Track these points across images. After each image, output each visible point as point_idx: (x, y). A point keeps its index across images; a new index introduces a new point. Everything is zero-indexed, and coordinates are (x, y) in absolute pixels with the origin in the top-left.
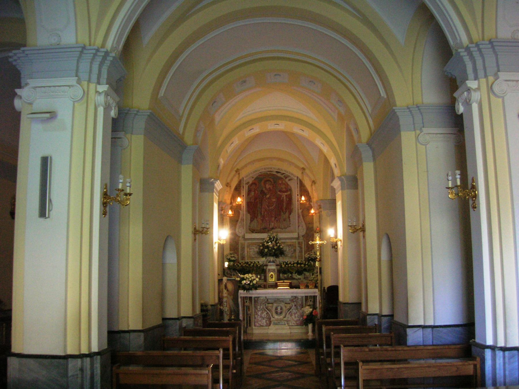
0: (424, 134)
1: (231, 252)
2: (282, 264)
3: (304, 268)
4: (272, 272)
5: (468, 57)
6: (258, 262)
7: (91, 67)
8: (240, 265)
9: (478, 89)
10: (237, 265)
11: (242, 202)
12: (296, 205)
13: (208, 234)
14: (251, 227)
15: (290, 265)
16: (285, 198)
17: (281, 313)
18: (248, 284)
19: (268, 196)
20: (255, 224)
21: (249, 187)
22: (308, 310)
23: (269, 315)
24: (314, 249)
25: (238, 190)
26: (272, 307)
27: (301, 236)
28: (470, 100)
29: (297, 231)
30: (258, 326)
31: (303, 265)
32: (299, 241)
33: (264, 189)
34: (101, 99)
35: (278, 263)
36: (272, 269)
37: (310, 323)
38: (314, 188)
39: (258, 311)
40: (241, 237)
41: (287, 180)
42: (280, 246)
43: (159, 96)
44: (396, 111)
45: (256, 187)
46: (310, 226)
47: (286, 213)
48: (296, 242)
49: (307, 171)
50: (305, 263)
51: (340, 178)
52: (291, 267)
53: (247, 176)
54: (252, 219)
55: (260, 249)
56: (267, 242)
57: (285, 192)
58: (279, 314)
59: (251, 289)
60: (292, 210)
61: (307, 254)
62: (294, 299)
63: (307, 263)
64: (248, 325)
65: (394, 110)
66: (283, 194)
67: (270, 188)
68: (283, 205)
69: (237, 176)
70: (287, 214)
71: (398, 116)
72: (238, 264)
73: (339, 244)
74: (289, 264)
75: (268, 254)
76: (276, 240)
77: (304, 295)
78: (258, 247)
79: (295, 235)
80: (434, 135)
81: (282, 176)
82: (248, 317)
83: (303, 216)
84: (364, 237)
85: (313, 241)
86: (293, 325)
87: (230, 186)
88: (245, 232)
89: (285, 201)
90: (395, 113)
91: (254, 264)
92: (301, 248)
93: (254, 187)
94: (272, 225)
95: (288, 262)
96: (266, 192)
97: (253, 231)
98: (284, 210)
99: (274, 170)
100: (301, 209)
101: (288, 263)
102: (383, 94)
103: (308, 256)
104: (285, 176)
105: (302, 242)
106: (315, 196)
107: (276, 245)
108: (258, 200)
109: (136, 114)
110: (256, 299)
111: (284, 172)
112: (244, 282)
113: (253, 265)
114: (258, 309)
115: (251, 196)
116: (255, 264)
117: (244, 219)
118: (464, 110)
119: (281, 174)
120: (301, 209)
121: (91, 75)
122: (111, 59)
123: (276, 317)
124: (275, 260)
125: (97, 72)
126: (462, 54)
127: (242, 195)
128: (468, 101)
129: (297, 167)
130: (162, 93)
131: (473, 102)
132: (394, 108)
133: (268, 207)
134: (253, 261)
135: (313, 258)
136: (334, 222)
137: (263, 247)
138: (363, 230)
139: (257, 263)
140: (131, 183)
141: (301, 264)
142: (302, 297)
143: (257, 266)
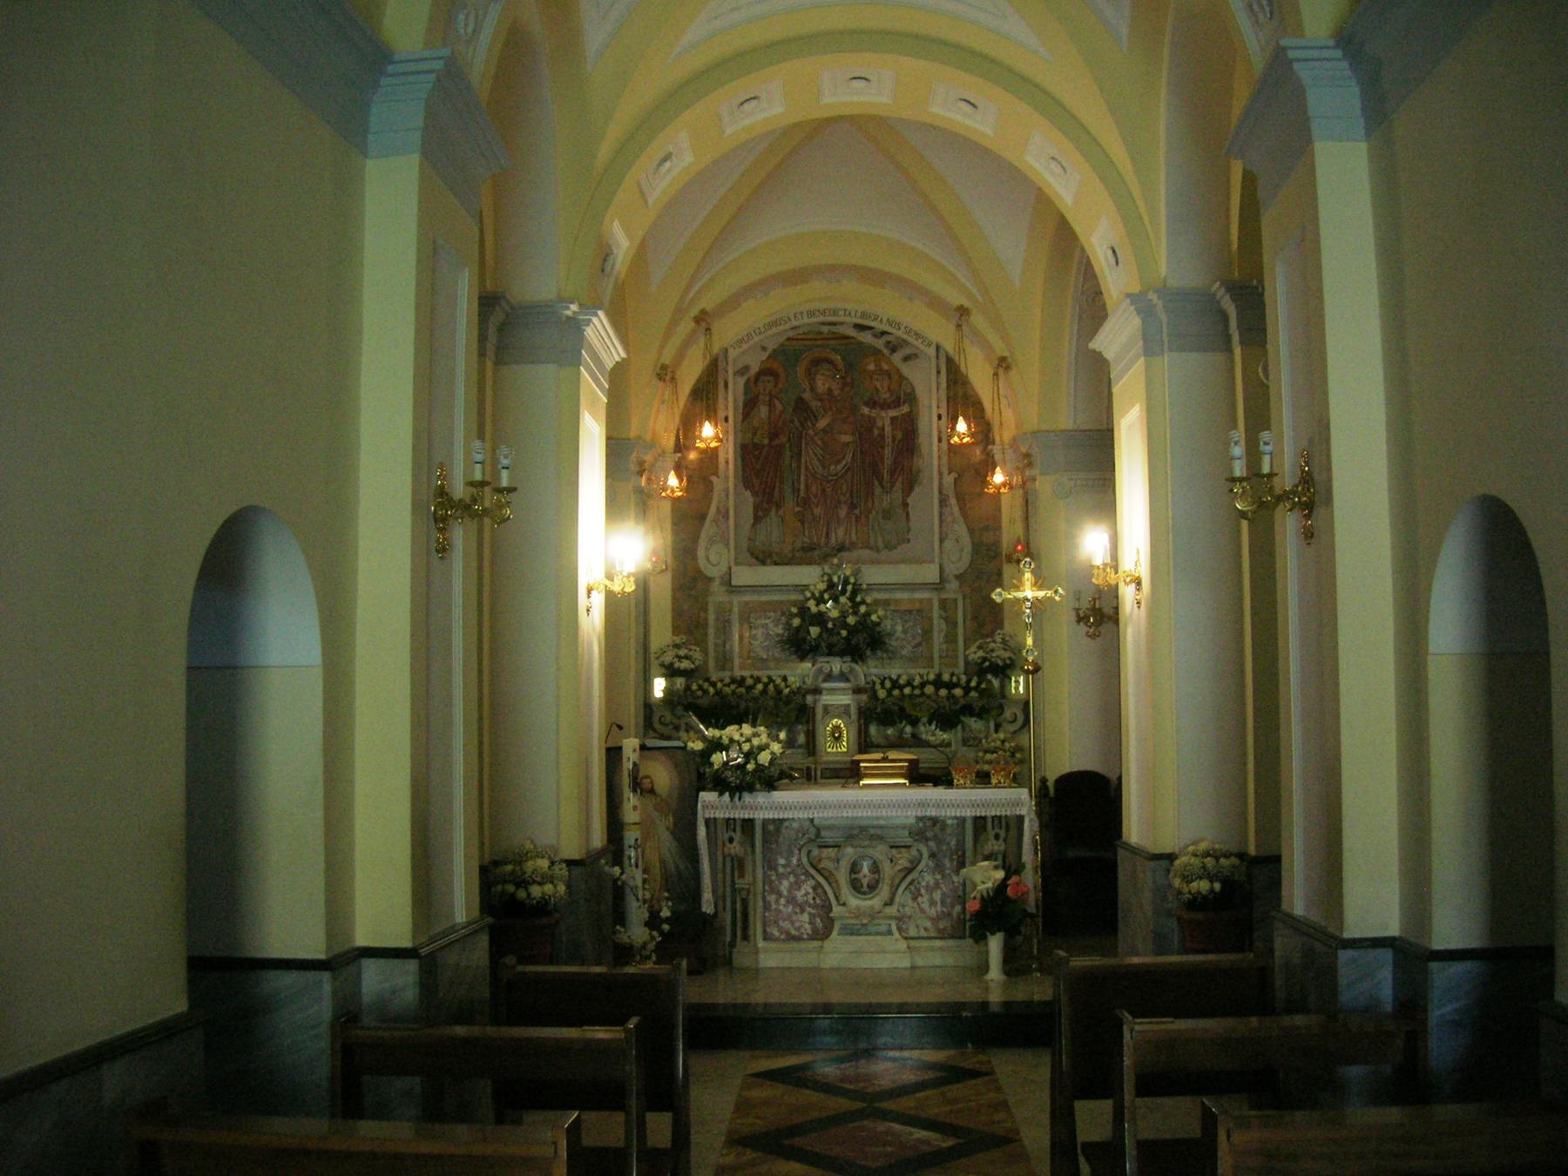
1: (678, 640)
2: (878, 687)
3: (962, 701)
6: (785, 679)
8: (711, 690)
10: (700, 687)
11: (720, 440)
15: (907, 691)
16: (888, 429)
17: (873, 887)
19: (822, 424)
20: (772, 532)
24: (1002, 629)
25: (704, 398)
27: (951, 578)
31: (958, 692)
32: (944, 596)
33: (807, 395)
35: (862, 682)
39: (781, 877)
41: (897, 358)
42: (868, 614)
45: (775, 387)
47: (895, 489)
48: (930, 601)
49: (978, 320)
50: (969, 681)
52: (911, 696)
54: (760, 513)
55: (788, 624)
56: (820, 601)
57: (889, 407)
61: (973, 648)
63: (973, 684)
64: (739, 933)
69: (702, 340)
70: (897, 494)
76: (855, 592)
77: (969, 813)
79: (930, 573)
81: (879, 344)
88: (732, 563)
89: (889, 440)
91: (766, 685)
92: (952, 623)
94: (839, 534)
95: (899, 676)
96: (814, 409)
97: (763, 557)
99: (847, 319)
101: (902, 682)
103: (981, 653)
106: (1007, 424)
107: (855, 613)
108: (783, 439)
112: (719, 758)
113: (765, 691)
114: (781, 870)
116: (771, 687)
117: (727, 511)
119: (875, 336)
123: (854, 902)
124: (852, 670)
127: (721, 414)
129: (936, 303)
134: (763, 675)
135: (1000, 663)
139: (778, 681)
141: (950, 686)
142: (962, 821)
143: (779, 691)
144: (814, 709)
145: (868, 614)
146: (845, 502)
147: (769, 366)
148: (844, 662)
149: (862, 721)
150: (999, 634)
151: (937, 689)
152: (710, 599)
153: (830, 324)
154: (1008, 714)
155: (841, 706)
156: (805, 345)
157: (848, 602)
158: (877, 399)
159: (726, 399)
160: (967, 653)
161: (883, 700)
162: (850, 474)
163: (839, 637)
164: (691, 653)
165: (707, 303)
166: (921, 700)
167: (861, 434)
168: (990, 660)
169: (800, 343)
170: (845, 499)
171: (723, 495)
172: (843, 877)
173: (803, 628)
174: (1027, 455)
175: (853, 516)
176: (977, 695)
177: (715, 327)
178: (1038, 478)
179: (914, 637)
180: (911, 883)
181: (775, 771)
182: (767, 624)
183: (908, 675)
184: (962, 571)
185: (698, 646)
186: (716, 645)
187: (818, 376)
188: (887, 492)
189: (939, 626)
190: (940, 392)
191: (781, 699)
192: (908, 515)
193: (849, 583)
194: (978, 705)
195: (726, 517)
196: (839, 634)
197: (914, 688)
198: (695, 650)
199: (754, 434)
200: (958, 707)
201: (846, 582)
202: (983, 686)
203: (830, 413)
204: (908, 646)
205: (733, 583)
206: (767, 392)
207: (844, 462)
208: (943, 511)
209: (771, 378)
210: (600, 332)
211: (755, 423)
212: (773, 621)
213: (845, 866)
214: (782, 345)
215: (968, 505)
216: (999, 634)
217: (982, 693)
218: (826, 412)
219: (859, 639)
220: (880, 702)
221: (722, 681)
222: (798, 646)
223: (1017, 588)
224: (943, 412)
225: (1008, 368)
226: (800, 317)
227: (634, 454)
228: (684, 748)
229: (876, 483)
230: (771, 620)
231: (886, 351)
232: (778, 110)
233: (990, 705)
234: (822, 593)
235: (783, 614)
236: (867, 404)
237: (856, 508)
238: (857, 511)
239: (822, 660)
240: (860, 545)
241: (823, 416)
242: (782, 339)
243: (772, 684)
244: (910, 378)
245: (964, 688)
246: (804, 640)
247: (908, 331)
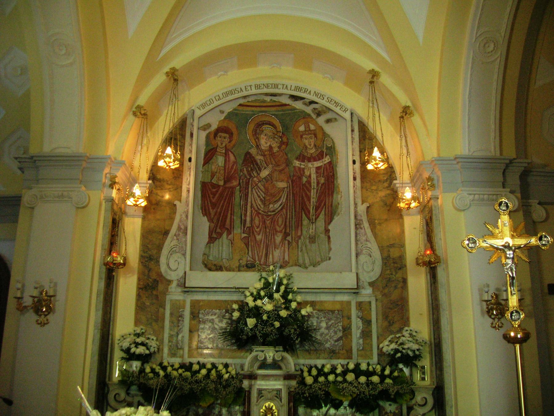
2: (306, 374)
3: (380, 388)
4: (271, 400)
8: (162, 373)
10: (153, 370)
14: (211, 258)
15: (331, 378)
16: (314, 176)
19: (265, 173)
21: (208, 137)
24: (409, 326)
27: (366, 284)
29: (354, 270)
32: (360, 299)
33: (253, 151)
35: (292, 369)
40: (174, 284)
41: (321, 121)
42: (297, 311)
45: (230, 142)
47: (318, 219)
48: (349, 303)
49: (385, 79)
50: (383, 370)
52: (335, 382)
54: (214, 235)
60: (337, 207)
61: (386, 343)
63: (387, 372)
66: (310, 165)
70: (321, 223)
74: (329, 373)
79: (349, 280)
81: (308, 110)
83: (372, 224)
88: (188, 269)
91: (209, 371)
92: (367, 322)
93: (222, 141)
95: (323, 366)
101: (326, 370)
103: (393, 346)
104: (314, 109)
107: (287, 308)
108: (235, 183)
111: (315, 99)
113: (208, 376)
115: (214, 168)
116: (213, 372)
117: (186, 229)
119: (305, 104)
124: (283, 358)
133: (263, 202)
135: (411, 354)
137: (242, 314)
139: (220, 367)
141: (369, 374)
143: (220, 376)
144: (249, 392)
146: (281, 232)
147: (225, 124)
148: (277, 351)
149: (292, 404)
150: (407, 330)
151: (357, 377)
152: (168, 297)
154: (419, 398)
155: (273, 390)
156: (253, 111)
157: (281, 299)
158: (306, 154)
159: (191, 145)
160: (381, 346)
161: (311, 385)
162: (284, 211)
163: (272, 328)
164: (147, 341)
165: (178, 62)
166: (345, 385)
167: (293, 181)
168: (401, 352)
169: (250, 108)
170: (281, 229)
171: (184, 216)
173: (242, 320)
174: (430, 179)
175: (286, 242)
176: (391, 381)
178: (440, 197)
179: (335, 333)
182: (213, 319)
183: (332, 365)
184: (374, 279)
185: (155, 336)
186: (171, 336)
187: (262, 136)
188: (313, 223)
190: (354, 144)
191: (220, 383)
192: (329, 238)
193: (283, 284)
194: (393, 391)
196: (273, 325)
198: (153, 339)
199: (213, 176)
200: (376, 393)
201: (280, 284)
202: (396, 374)
203: (270, 166)
204: (331, 340)
205: (187, 285)
206: (224, 145)
207: (280, 203)
208: (358, 232)
209: (227, 136)
211: (214, 168)
212: (218, 317)
214: (235, 109)
215: (378, 227)
216: (407, 330)
218: (268, 166)
219: (291, 331)
220: (308, 387)
221: (172, 366)
226: (250, 89)
227: (107, 170)
229: (304, 215)
230: (217, 316)
231: (314, 116)
236: (297, 159)
237: (289, 235)
238: (289, 238)
239: (257, 349)
240: (291, 264)
241: (265, 168)
242: (234, 105)
243: (214, 370)
244: (332, 136)
245: (379, 376)
246: (242, 331)
247: (330, 100)
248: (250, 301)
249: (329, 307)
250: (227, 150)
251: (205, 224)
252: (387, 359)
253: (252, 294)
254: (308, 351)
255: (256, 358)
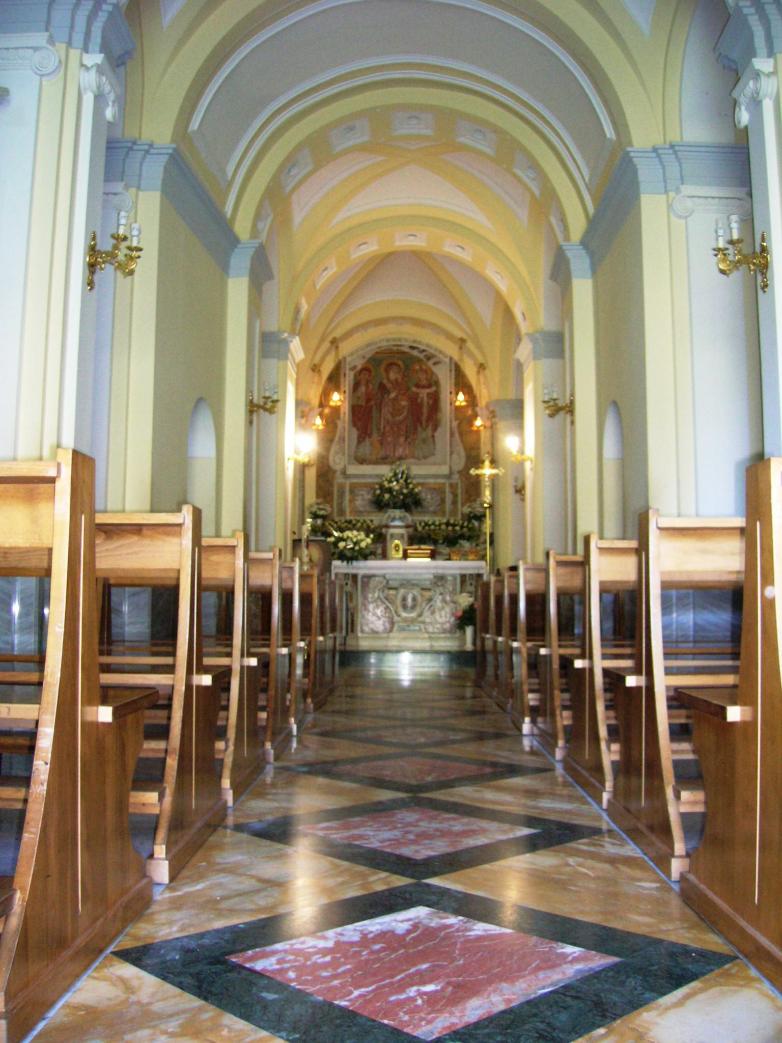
0: (684, 197)
1: (319, 501)
2: (418, 525)
3: (459, 533)
5: (756, 17)
6: (372, 521)
7: (73, 20)
9: (775, 73)
11: (342, 401)
12: (446, 412)
13: (274, 413)
15: (432, 527)
17: (413, 607)
18: (351, 549)
19: (393, 395)
20: (366, 449)
21: (355, 375)
22: (465, 600)
23: (390, 610)
25: (334, 380)
26: (396, 596)
28: (758, 94)
29: (448, 463)
30: (367, 633)
31: (458, 528)
33: (385, 381)
34: (90, 79)
36: (398, 534)
37: (468, 625)
38: (482, 380)
39: (369, 603)
41: (430, 363)
42: (413, 489)
43: (190, 130)
44: (632, 154)
45: (370, 376)
46: (474, 453)
48: (444, 484)
49: (470, 345)
51: (532, 337)
52: (434, 530)
53: (352, 354)
54: (361, 439)
55: (374, 494)
56: (390, 481)
58: (409, 609)
59: (356, 559)
61: (466, 507)
62: (440, 579)
64: (350, 630)
65: (628, 153)
67: (396, 380)
68: (422, 413)
69: (333, 353)
70: (429, 431)
71: (634, 166)
72: (332, 523)
73: (528, 465)
75: (391, 503)
76: (407, 478)
77: (457, 572)
78: (372, 491)
79: (445, 470)
80: (702, 200)
81: (421, 356)
82: (349, 614)
83: (461, 434)
84: (572, 423)
85: (477, 468)
86: (436, 630)
87: (319, 371)
88: (346, 463)
89: (425, 404)
90: (630, 160)
91: (362, 524)
92: (455, 495)
94: (400, 451)
97: (362, 461)
98: (424, 422)
100: (456, 419)
102: (610, 133)
103: (469, 510)
105: (457, 484)
106: (484, 396)
107: (407, 488)
108: (373, 403)
109: (147, 152)
110: (365, 580)
112: (342, 545)
114: (370, 600)
118: (750, 120)
120: (456, 419)
121: (74, 34)
122: (110, 8)
123: (404, 614)
124: (405, 517)
125: (84, 29)
126: (745, 11)
127: (343, 389)
128: (755, 95)
129: (449, 336)
130: (195, 125)
131: (765, 96)
132: (629, 149)
134: (361, 519)
136: (519, 427)
138: (570, 409)
139: (368, 522)
140: (141, 236)
141: (454, 525)
142: (455, 577)
145: (413, 489)
153: (398, 346)
165: (337, 333)
172: (399, 602)
173: (381, 495)
177: (340, 345)
180: (431, 606)
181: (368, 551)
186: (338, 504)
189: (449, 497)
194: (467, 534)
195: (344, 440)
196: (399, 498)
197: (436, 526)
201: (403, 473)
202: (470, 526)
209: (367, 372)
210: (296, 345)
213: (400, 597)
217: (470, 529)
219: (409, 500)
222: (379, 505)
223: (482, 468)
224: (453, 390)
225: (484, 369)
228: (325, 541)
232: (375, 248)
233: (473, 536)
234: (391, 478)
235: (372, 489)
238: (409, 440)
247: (436, 350)
248: (386, 484)
249: (433, 486)
250: (367, 382)
251: (355, 433)
252: (466, 518)
253: (387, 480)
254: (420, 512)
255: (389, 516)
